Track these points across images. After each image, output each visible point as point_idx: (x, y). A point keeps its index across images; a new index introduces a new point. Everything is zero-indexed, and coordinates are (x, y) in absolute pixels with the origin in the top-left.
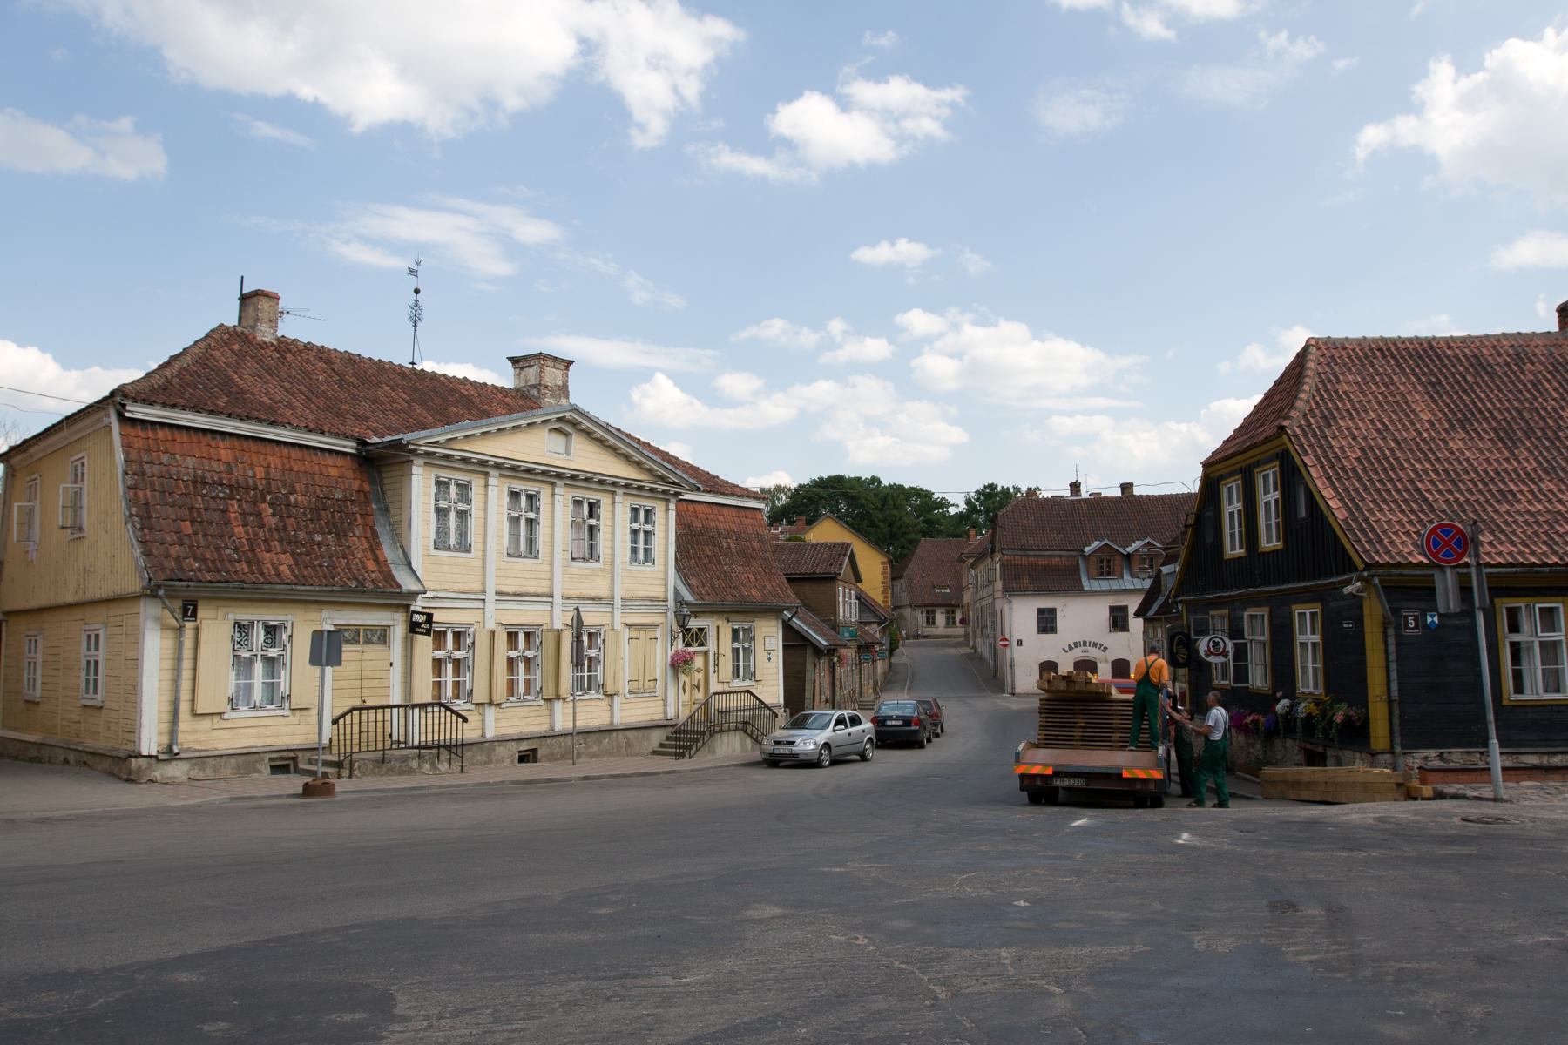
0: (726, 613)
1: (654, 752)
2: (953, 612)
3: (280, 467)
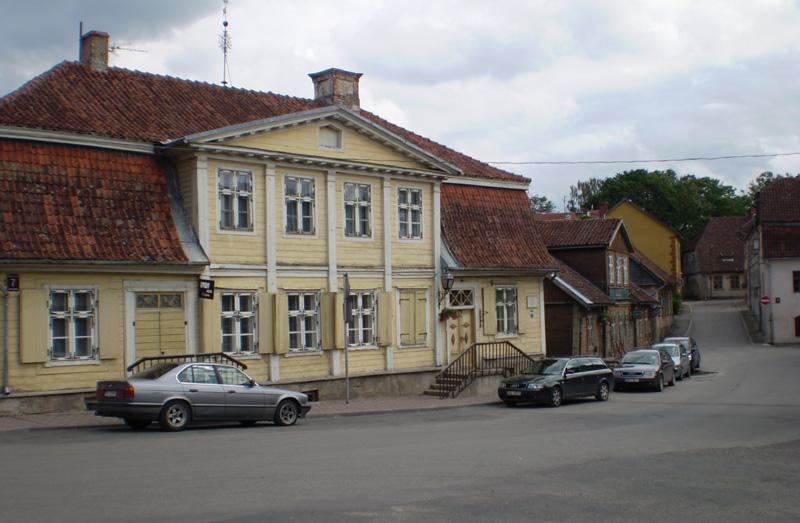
0: (491, 279)
1: (426, 393)
2: (738, 278)
3: (88, 166)
